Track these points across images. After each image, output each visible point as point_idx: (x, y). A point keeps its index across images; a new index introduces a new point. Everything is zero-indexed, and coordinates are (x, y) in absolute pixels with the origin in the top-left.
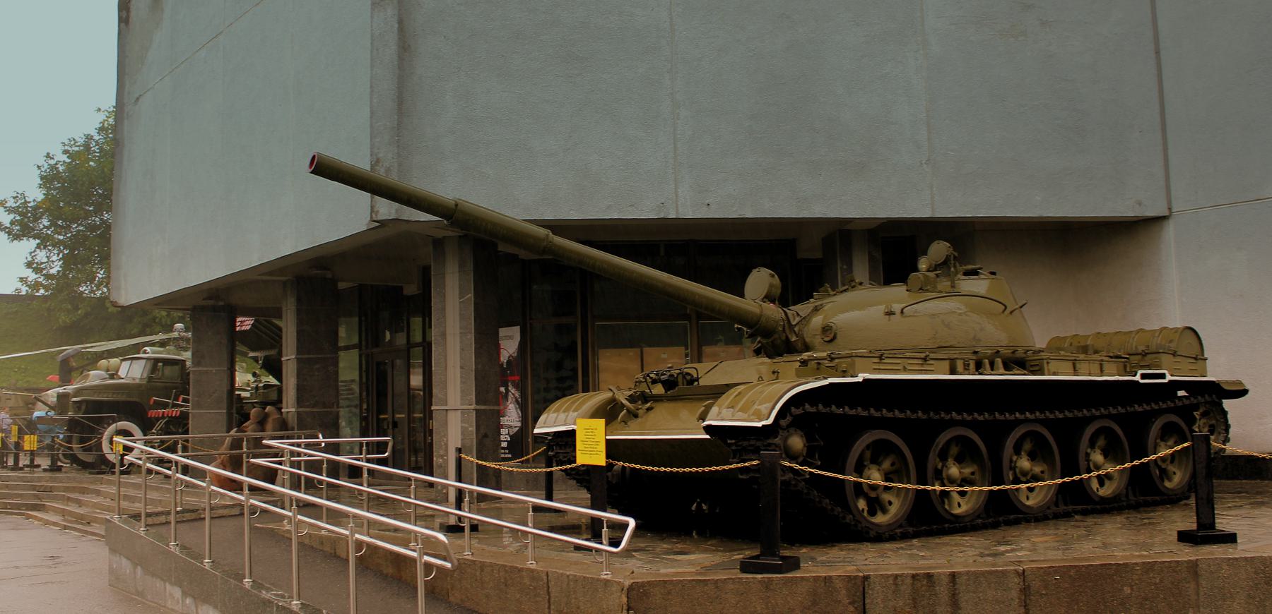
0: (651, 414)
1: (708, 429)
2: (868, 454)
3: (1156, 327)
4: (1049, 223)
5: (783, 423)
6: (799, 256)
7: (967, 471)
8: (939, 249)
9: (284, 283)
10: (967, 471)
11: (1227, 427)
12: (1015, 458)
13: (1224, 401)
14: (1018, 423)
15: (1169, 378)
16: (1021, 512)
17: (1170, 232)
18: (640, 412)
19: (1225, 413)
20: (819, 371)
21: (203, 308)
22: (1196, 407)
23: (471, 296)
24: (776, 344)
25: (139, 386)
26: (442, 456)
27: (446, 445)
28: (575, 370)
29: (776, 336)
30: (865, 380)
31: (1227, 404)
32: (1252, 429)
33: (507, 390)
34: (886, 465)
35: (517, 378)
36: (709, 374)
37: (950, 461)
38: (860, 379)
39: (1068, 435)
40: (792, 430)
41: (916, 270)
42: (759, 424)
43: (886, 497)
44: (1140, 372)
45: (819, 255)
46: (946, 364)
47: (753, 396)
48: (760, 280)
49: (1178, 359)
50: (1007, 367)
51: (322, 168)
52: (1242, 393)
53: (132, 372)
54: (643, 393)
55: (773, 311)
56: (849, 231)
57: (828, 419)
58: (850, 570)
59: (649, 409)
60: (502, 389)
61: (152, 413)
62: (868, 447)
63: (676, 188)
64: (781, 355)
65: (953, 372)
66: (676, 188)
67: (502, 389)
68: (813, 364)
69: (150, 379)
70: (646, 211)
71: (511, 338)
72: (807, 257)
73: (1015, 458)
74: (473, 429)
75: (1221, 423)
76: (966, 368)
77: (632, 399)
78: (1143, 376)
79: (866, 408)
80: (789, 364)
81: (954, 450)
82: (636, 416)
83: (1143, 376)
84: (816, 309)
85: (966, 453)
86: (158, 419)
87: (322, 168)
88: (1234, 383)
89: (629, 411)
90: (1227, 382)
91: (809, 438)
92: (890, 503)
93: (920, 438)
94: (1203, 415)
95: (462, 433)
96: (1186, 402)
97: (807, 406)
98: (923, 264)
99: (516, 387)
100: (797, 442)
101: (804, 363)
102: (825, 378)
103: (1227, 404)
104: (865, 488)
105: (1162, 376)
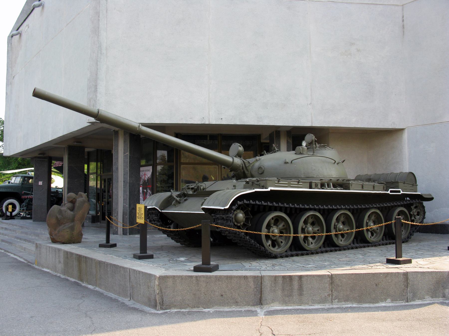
0: (187, 202)
1: (204, 209)
2: (273, 221)
3: (398, 172)
4: (359, 130)
5: (234, 207)
6: (262, 141)
7: (316, 229)
8: (310, 137)
9: (64, 148)
10: (316, 229)
11: (424, 213)
12: (336, 224)
13: (424, 202)
14: (337, 210)
15: (402, 192)
16: (370, 243)
17: (405, 135)
18: (181, 201)
19: (424, 207)
20: (253, 185)
21: (39, 157)
22: (412, 204)
23: (128, 153)
24: (239, 174)
25: (19, 186)
26: (116, 216)
27: (118, 212)
28: (173, 184)
29: (239, 171)
30: (271, 190)
31: (425, 203)
32: (434, 214)
33: (147, 191)
34: (281, 226)
35: (151, 187)
36: (206, 185)
37: (309, 225)
38: (269, 189)
39: (359, 214)
40: (238, 211)
41: (301, 145)
42: (223, 208)
43: (280, 240)
44: (390, 190)
45: (268, 141)
46: (308, 185)
47: (225, 195)
48: (237, 147)
49: (405, 185)
50: (335, 186)
51: (37, 94)
52: (432, 199)
53: (16, 181)
54: (184, 194)
55: (238, 161)
56: (279, 131)
57: (255, 207)
58: (257, 273)
59: (185, 200)
60: (145, 190)
61: (23, 197)
62: (273, 218)
63: (209, 112)
64: (240, 179)
65: (311, 188)
66: (209, 112)
67: (145, 190)
68: (250, 183)
69: (22, 184)
70: (196, 120)
71: (149, 170)
72: (258, 140)
73: (336, 224)
74: (128, 206)
75: (422, 212)
76: (316, 187)
77: (179, 196)
78: (391, 192)
79: (272, 202)
80: (242, 183)
81: (342, 219)
82: (179, 203)
83: (391, 192)
84: (257, 160)
85: (315, 222)
86: (25, 199)
87: (37, 94)
88: (428, 195)
89: (177, 201)
90: (425, 195)
91: (246, 214)
92: (282, 242)
93: (295, 214)
94: (416, 207)
95: (123, 207)
96: (409, 202)
97: (245, 201)
98: (304, 144)
99: (149, 189)
100: (241, 215)
101: (247, 183)
102: (254, 189)
103: (425, 203)
104: (271, 236)
105: (399, 192)
